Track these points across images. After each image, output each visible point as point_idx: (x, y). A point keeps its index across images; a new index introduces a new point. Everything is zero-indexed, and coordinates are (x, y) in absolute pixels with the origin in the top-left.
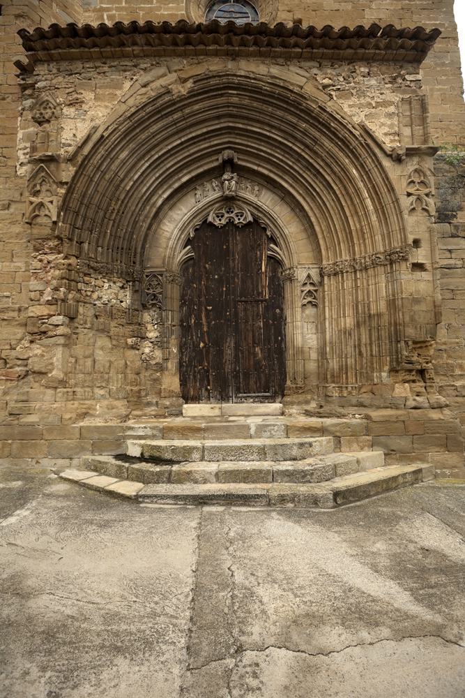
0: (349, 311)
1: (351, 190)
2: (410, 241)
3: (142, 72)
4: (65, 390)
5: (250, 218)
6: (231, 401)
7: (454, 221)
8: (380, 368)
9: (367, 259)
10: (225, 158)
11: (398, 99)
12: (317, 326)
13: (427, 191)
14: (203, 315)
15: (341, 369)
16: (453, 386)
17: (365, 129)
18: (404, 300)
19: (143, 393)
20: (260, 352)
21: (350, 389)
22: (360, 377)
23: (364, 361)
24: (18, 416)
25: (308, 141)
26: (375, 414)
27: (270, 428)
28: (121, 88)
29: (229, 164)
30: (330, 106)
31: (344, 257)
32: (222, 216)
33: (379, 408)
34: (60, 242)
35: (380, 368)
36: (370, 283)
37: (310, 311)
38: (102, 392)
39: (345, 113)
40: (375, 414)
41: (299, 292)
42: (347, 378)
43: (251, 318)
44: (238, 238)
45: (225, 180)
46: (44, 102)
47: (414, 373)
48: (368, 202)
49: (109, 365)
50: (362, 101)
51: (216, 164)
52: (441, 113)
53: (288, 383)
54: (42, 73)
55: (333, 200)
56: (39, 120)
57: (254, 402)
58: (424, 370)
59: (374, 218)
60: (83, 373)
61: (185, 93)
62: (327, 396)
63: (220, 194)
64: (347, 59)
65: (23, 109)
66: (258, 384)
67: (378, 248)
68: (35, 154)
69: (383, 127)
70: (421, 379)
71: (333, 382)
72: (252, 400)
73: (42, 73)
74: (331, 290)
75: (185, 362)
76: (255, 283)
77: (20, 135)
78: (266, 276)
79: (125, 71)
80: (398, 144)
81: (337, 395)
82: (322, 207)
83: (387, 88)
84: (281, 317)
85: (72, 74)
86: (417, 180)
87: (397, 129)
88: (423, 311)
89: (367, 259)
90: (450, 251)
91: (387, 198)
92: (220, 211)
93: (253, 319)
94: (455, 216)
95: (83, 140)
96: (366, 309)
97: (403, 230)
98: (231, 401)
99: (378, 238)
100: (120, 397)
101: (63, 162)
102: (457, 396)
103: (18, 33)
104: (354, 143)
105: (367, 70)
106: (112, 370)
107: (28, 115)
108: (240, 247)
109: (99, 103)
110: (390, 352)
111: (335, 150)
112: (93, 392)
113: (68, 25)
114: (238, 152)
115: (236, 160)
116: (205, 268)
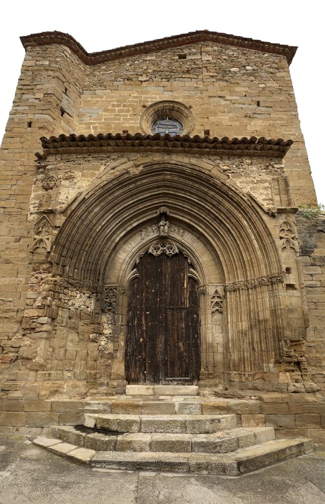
2: (284, 270)
3: (112, 161)
5: (177, 251)
7: (313, 255)
8: (268, 360)
9: (256, 281)
10: (162, 212)
12: (222, 327)
13: (293, 236)
15: (240, 360)
16: (322, 374)
19: (98, 376)
20: (182, 346)
21: (247, 376)
22: (254, 367)
25: (215, 203)
26: (266, 396)
27: (189, 406)
28: (98, 170)
29: (164, 216)
31: (240, 279)
32: (158, 249)
33: (268, 391)
35: (268, 360)
36: (258, 297)
37: (217, 316)
38: (69, 374)
39: (238, 186)
41: (210, 303)
45: (161, 225)
46: (50, 177)
47: (292, 364)
48: (255, 242)
50: (248, 179)
53: (202, 370)
54: (51, 160)
57: (177, 384)
62: (230, 381)
63: (157, 234)
65: (37, 180)
67: (263, 273)
70: (298, 369)
71: (235, 370)
72: (176, 383)
73: (51, 160)
75: (129, 353)
77: (32, 196)
78: (187, 291)
79: (102, 160)
80: (272, 206)
81: (238, 380)
82: (225, 245)
83: (263, 172)
84: (197, 321)
85: (69, 161)
86: (286, 229)
89: (256, 281)
90: (311, 275)
91: (267, 241)
93: (178, 322)
94: (313, 252)
96: (256, 316)
97: (279, 261)
99: (263, 266)
100: (82, 378)
103: (41, 139)
104: (244, 205)
105: (250, 162)
108: (169, 270)
109: (84, 178)
110: (274, 348)
111: (232, 209)
114: (170, 208)
115: (168, 213)
116: (146, 284)
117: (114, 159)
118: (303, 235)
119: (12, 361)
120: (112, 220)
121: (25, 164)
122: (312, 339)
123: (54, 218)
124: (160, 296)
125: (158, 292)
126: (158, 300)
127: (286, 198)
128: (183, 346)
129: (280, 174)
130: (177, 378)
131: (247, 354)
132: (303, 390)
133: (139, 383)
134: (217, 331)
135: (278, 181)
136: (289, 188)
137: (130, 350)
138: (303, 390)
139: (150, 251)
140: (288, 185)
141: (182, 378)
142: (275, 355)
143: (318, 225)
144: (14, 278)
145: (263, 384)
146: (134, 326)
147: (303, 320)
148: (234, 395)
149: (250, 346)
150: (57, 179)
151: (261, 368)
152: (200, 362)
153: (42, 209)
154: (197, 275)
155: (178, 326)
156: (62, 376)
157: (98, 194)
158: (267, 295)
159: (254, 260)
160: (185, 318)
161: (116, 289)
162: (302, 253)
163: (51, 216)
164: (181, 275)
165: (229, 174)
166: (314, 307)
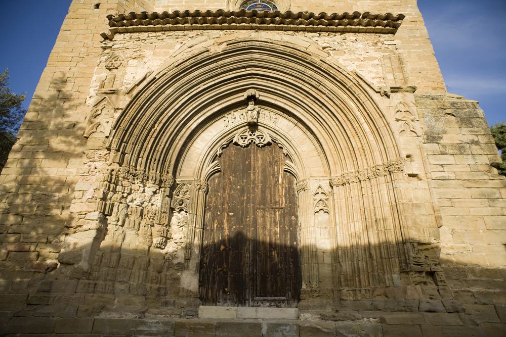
0: (358, 217)
1: (351, 117)
2: (404, 156)
3: (190, 39)
4: (87, 281)
5: (269, 140)
6: (247, 304)
7: (441, 141)
8: (390, 270)
9: (369, 172)
11: (380, 56)
12: (329, 232)
13: (412, 118)
14: (225, 221)
15: (353, 272)
16: (469, 291)
17: (357, 74)
18: (404, 205)
19: (162, 292)
20: (276, 256)
21: (363, 292)
22: (373, 280)
23: (375, 263)
24: (35, 307)
25: (314, 83)
26: (388, 317)
27: (282, 327)
28: (173, 48)
30: (328, 60)
31: (349, 170)
32: (246, 138)
33: (393, 311)
34: (108, 152)
35: (390, 270)
36: (374, 191)
37: (322, 216)
38: (122, 287)
39: (341, 64)
40: (388, 317)
41: (311, 200)
42: (360, 281)
43: (268, 224)
44: (259, 155)
46: (116, 57)
47: (424, 274)
48: (365, 126)
49: (133, 261)
50: (353, 56)
51: (243, 98)
52: (419, 67)
53: (304, 287)
54: (118, 39)
55: (337, 125)
56: (110, 68)
57: (270, 306)
58: (434, 272)
59: (371, 137)
60: (108, 267)
61: (220, 52)
62: (341, 299)
64: (339, 32)
65: (100, 62)
66: (275, 288)
67: (377, 161)
68: (102, 89)
69: (371, 74)
70: (432, 282)
71: (347, 285)
72: (268, 304)
73: (118, 39)
74: (340, 198)
75: (206, 263)
76: (273, 193)
77: (94, 78)
78: (282, 187)
79: (177, 38)
80: (384, 84)
81: (351, 298)
82: (328, 130)
83: (371, 49)
84: (296, 224)
85: (139, 40)
86: (403, 110)
87: (381, 75)
88: (424, 215)
89: (369, 172)
90: (442, 165)
91: (380, 122)
92: (244, 134)
93: (271, 225)
94: (441, 138)
95: (139, 81)
96: (373, 214)
97: (396, 146)
98: (247, 304)
99: (377, 153)
100: (139, 293)
101: (122, 95)
102: (476, 303)
103: (107, 17)
104: (349, 84)
105: (355, 38)
106: (135, 266)
107: (103, 65)
108: (260, 162)
109: (156, 58)
110: (398, 253)
111: (336, 89)
112: (113, 287)
113: (143, 12)
115: (257, 96)
116: (229, 179)
117: (192, 38)
118: (427, 119)
119: (49, 270)
120: (182, 75)
121: (88, 46)
122: (450, 244)
123: (117, 100)
124: (248, 194)
125: (245, 188)
126: (245, 198)
127: (401, 77)
128: (278, 256)
129: (392, 51)
130: (270, 298)
131: (362, 264)
132: (441, 308)
133: (218, 304)
134: (322, 236)
135: (390, 58)
136: (404, 65)
137: (206, 260)
138: (441, 308)
139: (235, 140)
140: (403, 62)
141: (276, 298)
142: (400, 263)
143: (445, 108)
144: (62, 170)
145: (386, 301)
146: (212, 230)
147: (434, 218)
148: (347, 317)
149: (366, 253)
150: (124, 58)
151: (381, 281)
152: (301, 278)
153: (103, 90)
154: (295, 168)
155: (271, 230)
156: (112, 288)
157: (171, 73)
158: (384, 188)
159: (366, 147)
160: (280, 221)
161: (190, 184)
162: (427, 139)
163: (114, 97)
164: (274, 168)
165: (330, 51)
166: (449, 204)
